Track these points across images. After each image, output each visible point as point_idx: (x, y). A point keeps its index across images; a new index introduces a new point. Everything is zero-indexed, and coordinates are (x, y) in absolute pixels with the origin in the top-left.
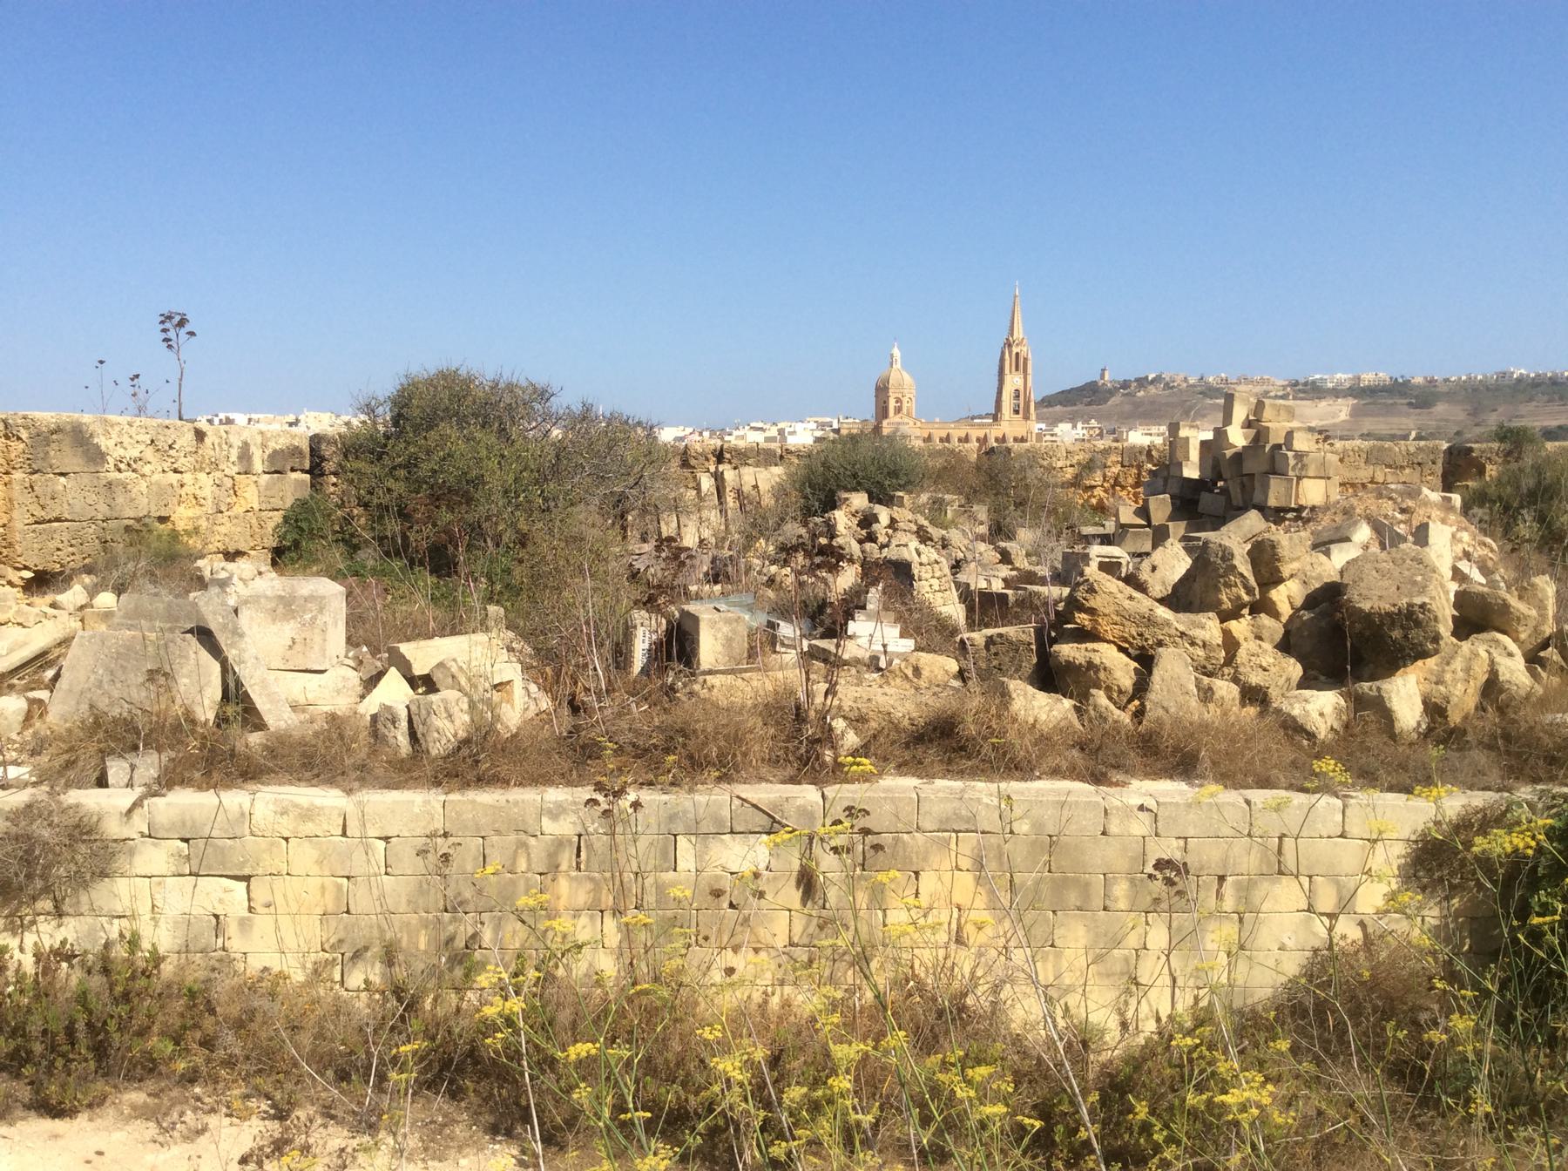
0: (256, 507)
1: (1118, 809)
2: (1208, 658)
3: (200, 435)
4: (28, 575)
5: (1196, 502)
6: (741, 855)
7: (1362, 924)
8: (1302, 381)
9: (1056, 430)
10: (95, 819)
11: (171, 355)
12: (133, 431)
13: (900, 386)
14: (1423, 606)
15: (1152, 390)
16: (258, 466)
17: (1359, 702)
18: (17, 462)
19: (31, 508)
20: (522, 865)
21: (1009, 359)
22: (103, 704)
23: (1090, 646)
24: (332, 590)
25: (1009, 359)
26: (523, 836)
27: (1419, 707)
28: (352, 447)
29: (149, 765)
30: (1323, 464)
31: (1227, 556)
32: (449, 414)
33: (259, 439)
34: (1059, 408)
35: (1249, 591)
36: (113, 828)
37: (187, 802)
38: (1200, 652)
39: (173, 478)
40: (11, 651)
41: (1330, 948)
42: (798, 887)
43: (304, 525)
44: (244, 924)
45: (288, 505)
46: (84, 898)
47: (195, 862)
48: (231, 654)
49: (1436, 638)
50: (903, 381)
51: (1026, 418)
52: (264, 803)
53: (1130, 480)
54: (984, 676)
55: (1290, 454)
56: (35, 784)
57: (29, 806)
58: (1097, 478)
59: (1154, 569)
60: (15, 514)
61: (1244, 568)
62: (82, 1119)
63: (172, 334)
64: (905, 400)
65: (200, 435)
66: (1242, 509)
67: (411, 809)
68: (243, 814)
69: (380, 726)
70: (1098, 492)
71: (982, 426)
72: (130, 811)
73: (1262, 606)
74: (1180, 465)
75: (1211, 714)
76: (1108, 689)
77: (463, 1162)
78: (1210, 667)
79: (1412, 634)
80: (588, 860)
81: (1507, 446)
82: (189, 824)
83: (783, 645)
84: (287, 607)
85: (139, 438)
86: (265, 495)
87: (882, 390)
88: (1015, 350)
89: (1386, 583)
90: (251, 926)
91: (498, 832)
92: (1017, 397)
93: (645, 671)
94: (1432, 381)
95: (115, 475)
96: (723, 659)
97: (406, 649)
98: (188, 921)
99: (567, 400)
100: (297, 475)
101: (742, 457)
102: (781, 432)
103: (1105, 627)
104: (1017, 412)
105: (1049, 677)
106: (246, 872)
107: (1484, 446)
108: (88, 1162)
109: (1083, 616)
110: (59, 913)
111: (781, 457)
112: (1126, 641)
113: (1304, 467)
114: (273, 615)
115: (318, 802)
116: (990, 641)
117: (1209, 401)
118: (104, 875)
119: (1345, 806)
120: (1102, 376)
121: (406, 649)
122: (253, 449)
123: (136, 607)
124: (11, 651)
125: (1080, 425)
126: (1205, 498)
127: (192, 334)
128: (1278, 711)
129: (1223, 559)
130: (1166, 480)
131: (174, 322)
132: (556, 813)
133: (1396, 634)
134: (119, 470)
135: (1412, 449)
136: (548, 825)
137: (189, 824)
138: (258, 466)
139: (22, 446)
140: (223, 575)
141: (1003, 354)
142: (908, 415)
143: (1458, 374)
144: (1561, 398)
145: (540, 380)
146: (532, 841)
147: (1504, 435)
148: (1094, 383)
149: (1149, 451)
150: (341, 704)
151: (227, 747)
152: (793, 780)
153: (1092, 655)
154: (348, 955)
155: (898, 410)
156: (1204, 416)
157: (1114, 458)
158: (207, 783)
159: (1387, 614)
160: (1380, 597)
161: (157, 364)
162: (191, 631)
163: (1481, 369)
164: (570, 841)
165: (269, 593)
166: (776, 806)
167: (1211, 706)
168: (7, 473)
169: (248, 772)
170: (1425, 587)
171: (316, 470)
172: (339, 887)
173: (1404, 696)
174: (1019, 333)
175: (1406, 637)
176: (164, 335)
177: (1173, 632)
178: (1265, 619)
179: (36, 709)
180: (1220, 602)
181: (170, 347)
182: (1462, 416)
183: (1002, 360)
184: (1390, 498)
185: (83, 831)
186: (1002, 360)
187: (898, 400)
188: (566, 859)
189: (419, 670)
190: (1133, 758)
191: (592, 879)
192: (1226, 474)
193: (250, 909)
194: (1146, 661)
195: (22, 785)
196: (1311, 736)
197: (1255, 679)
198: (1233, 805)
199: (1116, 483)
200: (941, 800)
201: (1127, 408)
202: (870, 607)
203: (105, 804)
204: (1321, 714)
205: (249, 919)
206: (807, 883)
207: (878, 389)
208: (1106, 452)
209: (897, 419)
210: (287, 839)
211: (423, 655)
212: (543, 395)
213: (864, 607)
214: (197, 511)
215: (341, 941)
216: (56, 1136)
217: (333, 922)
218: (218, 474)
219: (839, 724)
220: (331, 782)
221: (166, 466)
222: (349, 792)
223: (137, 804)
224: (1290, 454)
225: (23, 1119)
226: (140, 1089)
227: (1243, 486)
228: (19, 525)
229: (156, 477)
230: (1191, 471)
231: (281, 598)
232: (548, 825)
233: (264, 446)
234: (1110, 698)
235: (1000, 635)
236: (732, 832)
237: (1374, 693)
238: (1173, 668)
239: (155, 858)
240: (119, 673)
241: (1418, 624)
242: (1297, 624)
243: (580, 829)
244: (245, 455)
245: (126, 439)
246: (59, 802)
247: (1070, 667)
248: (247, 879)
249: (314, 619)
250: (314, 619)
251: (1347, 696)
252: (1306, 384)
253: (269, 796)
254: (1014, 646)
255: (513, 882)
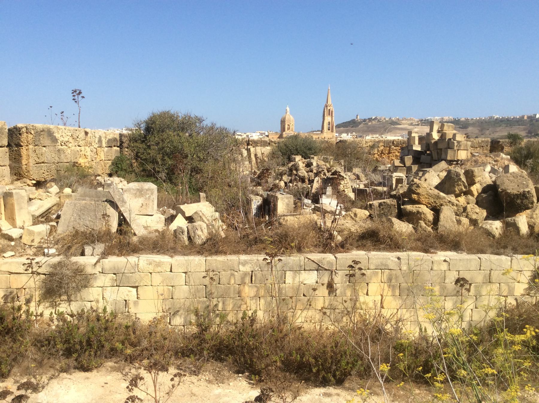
0: (104, 159)
1: (436, 261)
2: (458, 210)
3: (86, 133)
4: (34, 182)
5: (420, 158)
6: (310, 278)
7: (516, 299)
8: (424, 119)
9: (342, 136)
10: (82, 267)
11: (76, 104)
12: (66, 131)
13: (289, 120)
14: (528, 192)
15: (374, 122)
16: (104, 145)
17: (507, 225)
18: (30, 142)
19: (35, 158)
20: (232, 282)
21: (327, 111)
22: (77, 227)
23: (417, 206)
24: (154, 187)
25: (327, 111)
26: (233, 272)
27: (527, 226)
28: (133, 139)
29: (100, 248)
30: (466, 145)
31: (458, 175)
32: (168, 127)
33: (104, 135)
34: (342, 128)
35: (465, 187)
36: (89, 270)
37: (113, 261)
38: (455, 208)
39: (78, 148)
40: (38, 209)
41: (505, 308)
42: (327, 289)
43: (120, 166)
44: (136, 303)
45: (113, 158)
46: (79, 295)
47: (118, 282)
48: (122, 209)
49: (532, 203)
50: (290, 118)
51: (332, 131)
52: (144, 260)
53: (387, 152)
54: (380, 216)
55: (455, 142)
56: (58, 255)
57: (60, 263)
58: (376, 151)
59: (426, 180)
60: (30, 160)
61: (463, 179)
62: (95, 372)
63: (76, 97)
64: (291, 125)
65: (86, 133)
66: (439, 160)
67: (198, 262)
68: (136, 265)
69: (177, 234)
70: (376, 156)
71: (318, 134)
72: (95, 264)
73: (468, 193)
74: (412, 146)
75: (461, 229)
76: (424, 220)
77: (231, 384)
78: (458, 213)
79: (524, 201)
80: (255, 280)
81: (511, 140)
82: (116, 268)
83: (306, 206)
84: (140, 193)
85: (68, 134)
86: (106, 155)
87: (283, 122)
88: (328, 108)
89: (513, 184)
90: (138, 304)
91: (224, 270)
92: (329, 124)
93: (256, 215)
94: (467, 119)
95: (60, 147)
96: (286, 211)
97: (182, 207)
98: (115, 302)
99: (207, 123)
100: (116, 148)
101: (256, 143)
102: (248, 136)
103: (422, 199)
104: (329, 130)
105: (402, 215)
106: (137, 285)
107: (504, 140)
108: (103, 387)
109: (415, 195)
110: (69, 301)
111: (269, 144)
112: (430, 204)
113: (460, 146)
114: (135, 196)
115: (162, 260)
116: (380, 204)
117: (393, 126)
118: (86, 287)
119: (512, 259)
120: (357, 118)
121: (182, 207)
122: (102, 138)
123: (84, 193)
124: (38, 209)
125: (349, 134)
126: (423, 157)
127: (83, 97)
128: (482, 227)
129: (457, 176)
130: (409, 151)
131: (77, 93)
132: (244, 263)
133: (519, 201)
134: (62, 145)
135: (480, 141)
136: (242, 268)
137: (116, 268)
138: (104, 145)
139: (32, 136)
140: (109, 182)
141: (324, 109)
142: (292, 130)
143: (476, 117)
144: (510, 125)
145: (199, 115)
146: (236, 273)
147: (510, 136)
148: (354, 120)
149: (393, 142)
150: (161, 226)
151: (122, 240)
152: (323, 252)
153: (419, 209)
154: (172, 314)
155: (289, 129)
156: (391, 131)
157: (381, 144)
158: (121, 254)
159: (516, 194)
160: (513, 189)
161: (70, 107)
162: (106, 201)
163: (484, 115)
164: (249, 273)
165: (134, 188)
166: (320, 261)
167: (461, 226)
168: (27, 146)
169: (135, 250)
170: (528, 185)
171: (121, 146)
172: (169, 289)
173: (522, 221)
174: (330, 102)
175: (522, 202)
176: (73, 98)
177: (446, 201)
178: (470, 197)
179: (53, 230)
180: (455, 191)
181: (76, 102)
182: (477, 131)
183: (324, 112)
184: (490, 157)
185: (79, 271)
186: (324, 112)
187: (289, 125)
188: (248, 280)
189: (187, 215)
190: (437, 244)
191: (256, 286)
192: (432, 149)
193: (138, 298)
194: (436, 211)
195: (53, 255)
196: (494, 237)
197: (474, 217)
198: (475, 259)
199: (382, 153)
200: (376, 259)
201: (365, 128)
202: (327, 193)
203: (88, 261)
204: (497, 229)
205: (137, 301)
206: (330, 286)
207: (281, 121)
208: (379, 142)
209: (288, 132)
210: (151, 273)
211: (189, 209)
212: (200, 120)
213: (325, 194)
214: (86, 160)
215: (169, 308)
216: (88, 378)
217: (167, 302)
218: (92, 147)
219: (335, 233)
220: (164, 253)
221: (76, 144)
222: (172, 257)
223: (98, 261)
224: (455, 142)
225: (74, 372)
226: (111, 361)
227: (438, 153)
228: (31, 164)
229: (73, 148)
230: (417, 147)
231: (138, 189)
232: (242, 268)
233: (106, 137)
234: (426, 224)
235: (384, 202)
236: (304, 270)
237: (513, 221)
238: (447, 215)
239: (105, 280)
240: (82, 216)
241: (527, 198)
242: (480, 199)
243: (252, 269)
244: (100, 141)
245: (64, 135)
246: (70, 261)
247: (411, 213)
248: (137, 287)
249: (150, 197)
250: (150, 197)
251: (503, 222)
252: (425, 120)
253: (144, 258)
254: (389, 206)
255: (229, 288)
